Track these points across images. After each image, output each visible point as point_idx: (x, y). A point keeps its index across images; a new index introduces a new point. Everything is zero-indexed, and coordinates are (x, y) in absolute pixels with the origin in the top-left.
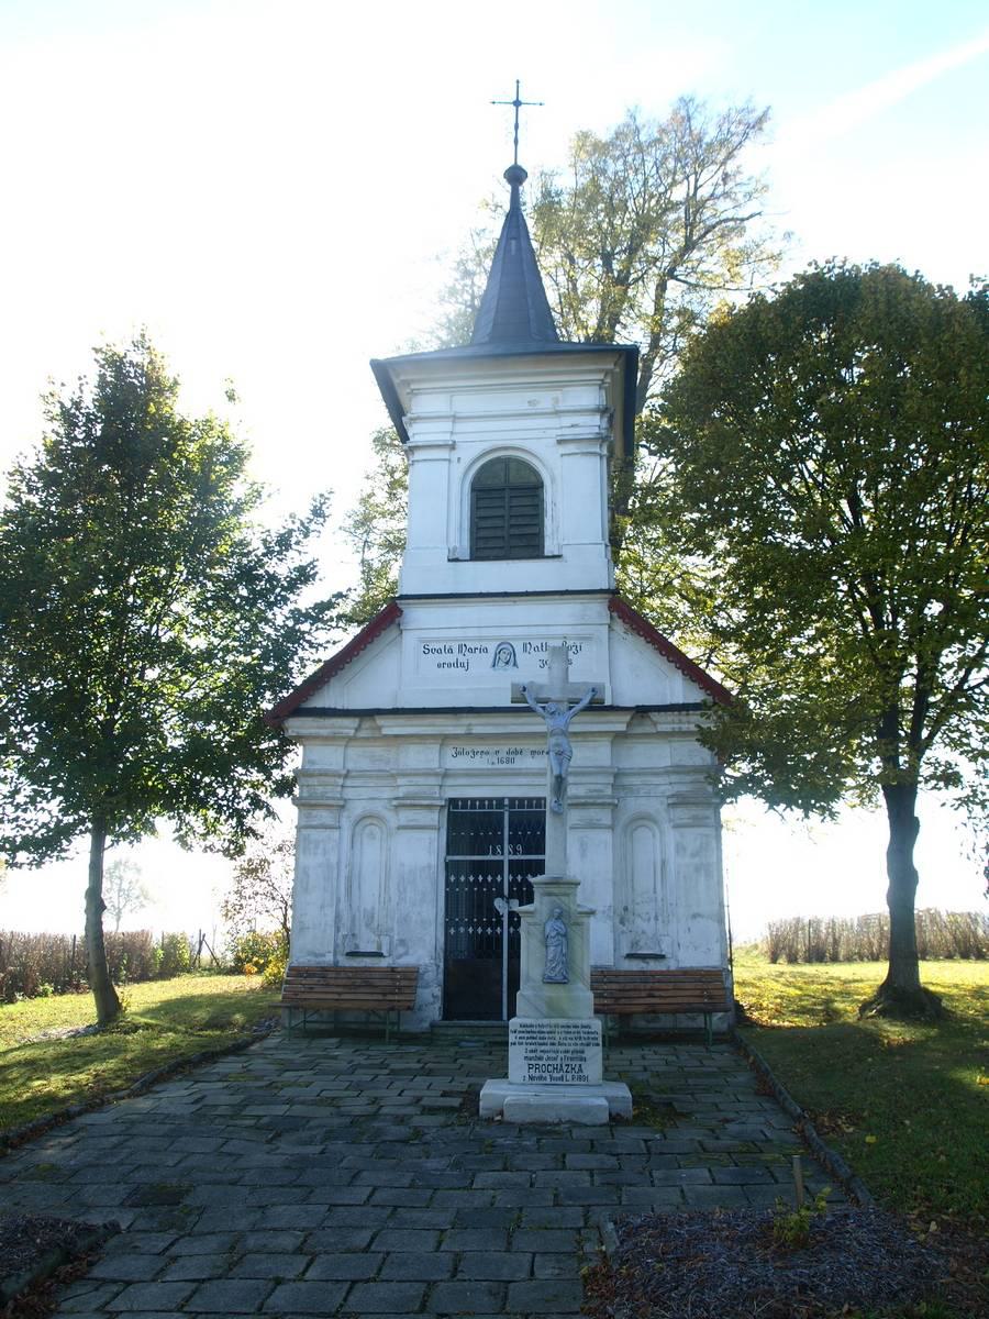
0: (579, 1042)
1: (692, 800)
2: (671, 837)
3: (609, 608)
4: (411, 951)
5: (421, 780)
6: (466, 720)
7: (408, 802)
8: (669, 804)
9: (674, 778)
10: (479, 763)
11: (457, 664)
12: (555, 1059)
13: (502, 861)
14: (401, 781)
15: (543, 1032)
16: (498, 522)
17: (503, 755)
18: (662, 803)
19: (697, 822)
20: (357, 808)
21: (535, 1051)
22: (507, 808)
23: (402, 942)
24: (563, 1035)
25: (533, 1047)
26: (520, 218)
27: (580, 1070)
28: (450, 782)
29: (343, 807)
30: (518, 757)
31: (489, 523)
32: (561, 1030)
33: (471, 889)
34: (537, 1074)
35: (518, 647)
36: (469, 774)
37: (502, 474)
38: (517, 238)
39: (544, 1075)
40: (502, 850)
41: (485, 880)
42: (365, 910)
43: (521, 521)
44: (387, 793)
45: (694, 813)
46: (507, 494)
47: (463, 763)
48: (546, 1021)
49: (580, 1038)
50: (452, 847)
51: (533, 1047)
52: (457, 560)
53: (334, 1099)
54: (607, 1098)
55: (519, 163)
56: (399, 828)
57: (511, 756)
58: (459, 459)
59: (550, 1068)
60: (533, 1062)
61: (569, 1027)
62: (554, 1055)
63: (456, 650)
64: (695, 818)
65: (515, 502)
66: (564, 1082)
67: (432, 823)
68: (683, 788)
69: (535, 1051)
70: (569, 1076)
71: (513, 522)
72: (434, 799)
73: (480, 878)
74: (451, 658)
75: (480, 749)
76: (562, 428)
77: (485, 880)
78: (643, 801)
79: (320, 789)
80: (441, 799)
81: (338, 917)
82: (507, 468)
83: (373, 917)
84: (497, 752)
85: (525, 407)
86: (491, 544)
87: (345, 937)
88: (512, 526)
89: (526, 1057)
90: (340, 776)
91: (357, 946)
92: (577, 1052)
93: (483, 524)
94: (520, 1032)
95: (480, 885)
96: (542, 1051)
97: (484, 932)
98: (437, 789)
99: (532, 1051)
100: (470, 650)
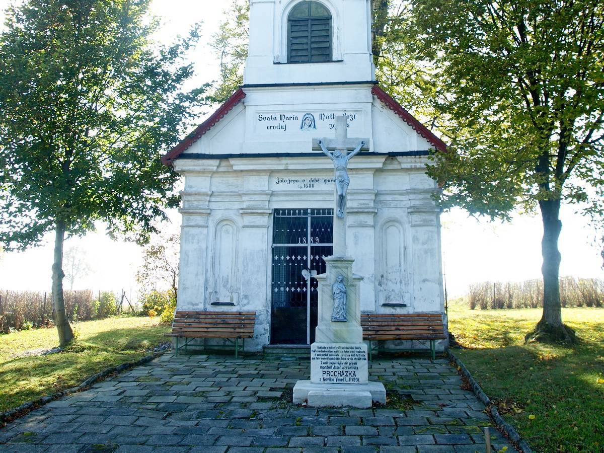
0: (353, 357)
2: (410, 232)
5: (257, 198)
6: (285, 161)
7: (249, 211)
8: (408, 213)
9: (412, 196)
10: (293, 187)
11: (279, 127)
12: (339, 368)
13: (306, 248)
14: (244, 198)
15: (332, 352)
16: (305, 40)
17: (306, 182)
18: (404, 212)
19: (425, 223)
20: (218, 215)
21: (327, 363)
22: (309, 215)
23: (246, 297)
24: (344, 353)
25: (326, 361)
27: (354, 374)
28: (275, 198)
29: (210, 214)
30: (316, 184)
32: (344, 350)
34: (328, 377)
36: (286, 194)
37: (307, 11)
39: (332, 378)
41: (296, 258)
42: (223, 277)
43: (318, 40)
44: (237, 206)
45: (424, 217)
46: (310, 21)
47: (283, 187)
48: (333, 345)
51: (326, 361)
57: (312, 183)
59: (336, 374)
62: (338, 366)
63: (278, 118)
65: (315, 28)
66: (345, 382)
68: (417, 203)
69: (327, 363)
70: (348, 378)
71: (313, 40)
73: (293, 258)
74: (275, 123)
77: (296, 258)
80: (269, 209)
81: (206, 281)
83: (228, 279)
84: (304, 181)
86: (300, 53)
87: (211, 293)
88: (312, 42)
90: (207, 195)
91: (218, 299)
95: (293, 262)
99: (325, 363)
100: (288, 118)
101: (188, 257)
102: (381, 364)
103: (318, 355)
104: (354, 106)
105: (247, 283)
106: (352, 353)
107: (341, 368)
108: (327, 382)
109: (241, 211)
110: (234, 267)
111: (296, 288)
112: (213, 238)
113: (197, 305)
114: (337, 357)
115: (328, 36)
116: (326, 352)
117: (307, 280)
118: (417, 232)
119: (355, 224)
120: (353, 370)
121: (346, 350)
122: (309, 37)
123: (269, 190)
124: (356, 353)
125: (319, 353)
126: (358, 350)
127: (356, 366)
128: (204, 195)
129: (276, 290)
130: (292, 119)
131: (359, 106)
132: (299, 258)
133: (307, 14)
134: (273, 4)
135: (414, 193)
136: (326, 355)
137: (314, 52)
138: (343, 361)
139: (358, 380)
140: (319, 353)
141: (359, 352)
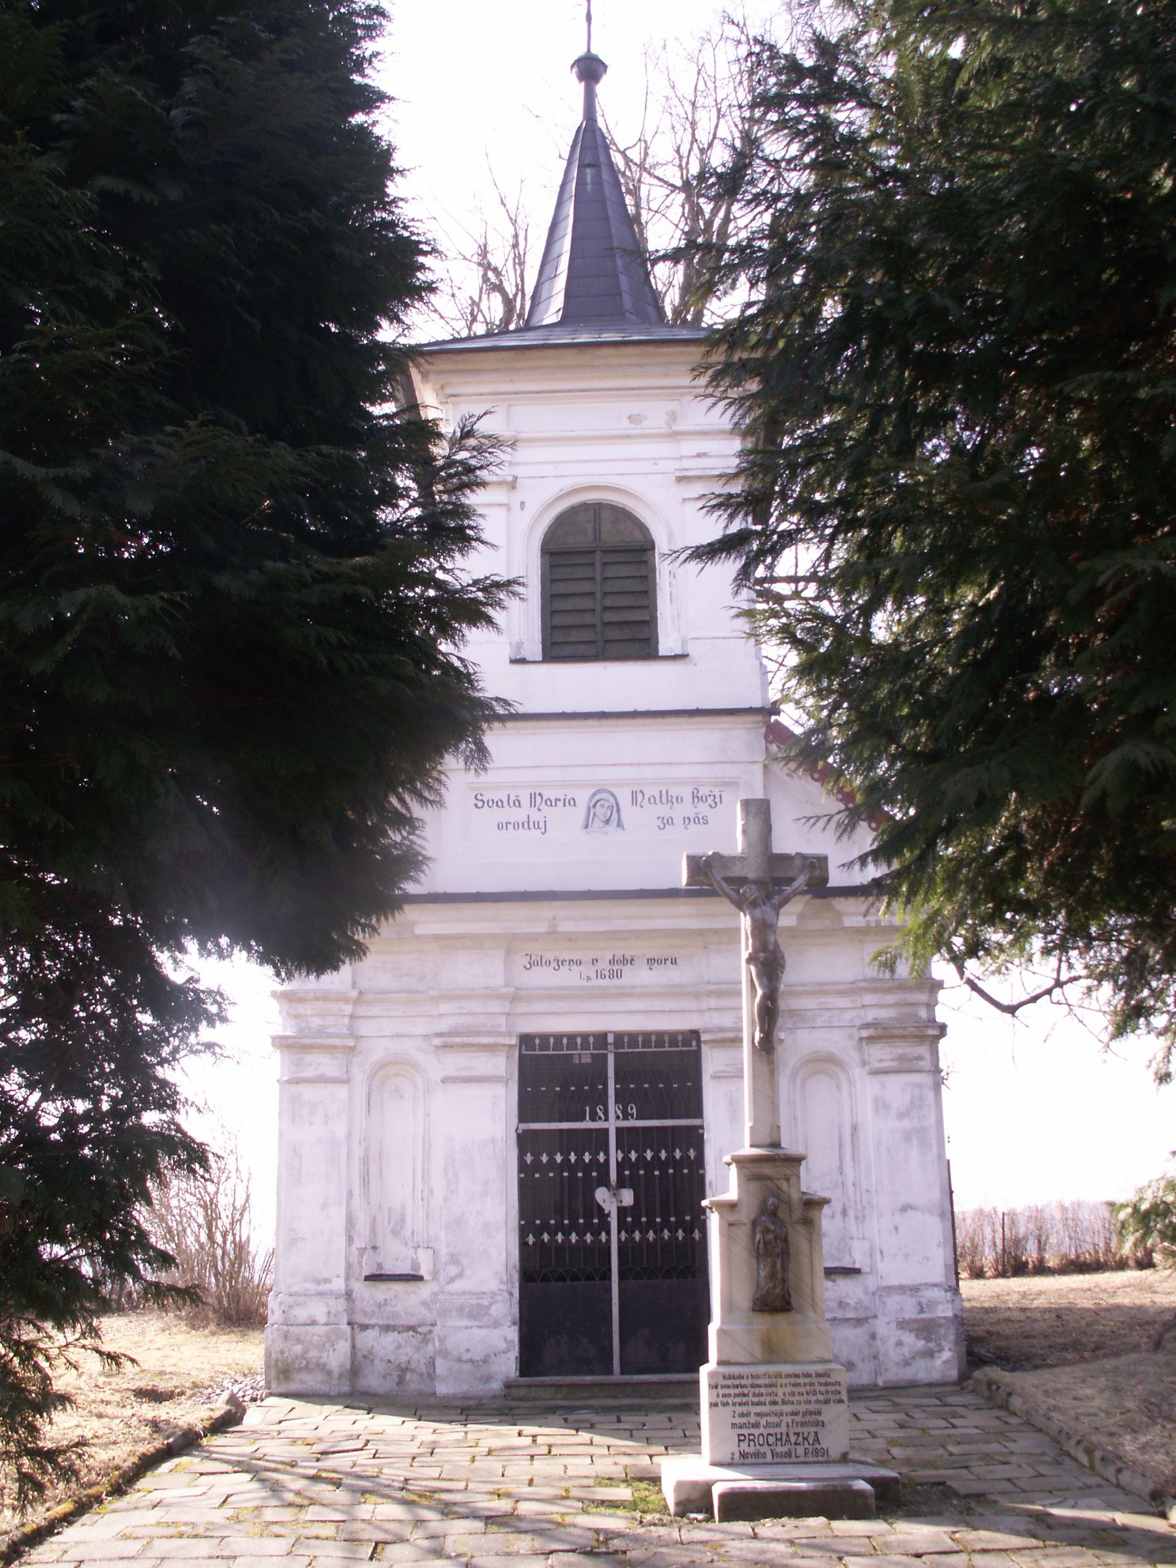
0: (813, 1398)
1: (896, 1032)
2: (867, 1088)
3: (766, 737)
4: (467, 1272)
5: (476, 1006)
6: (547, 911)
7: (458, 1040)
8: (861, 1039)
9: (869, 999)
10: (568, 977)
11: (527, 824)
12: (778, 1425)
13: (607, 1130)
14: (445, 1008)
15: (758, 1386)
16: (587, 603)
17: (603, 965)
18: (850, 1037)
19: (905, 1067)
20: (377, 1051)
21: (748, 1414)
22: (611, 1048)
23: (454, 1260)
24: (789, 1389)
25: (744, 1409)
26: (598, 132)
27: (817, 1440)
28: (522, 1008)
29: (352, 1049)
30: (627, 969)
31: (570, 604)
32: (787, 1381)
33: (573, 1175)
34: (752, 1449)
35: (624, 798)
36: (553, 995)
37: (590, 527)
38: (595, 165)
39: (762, 1450)
40: (606, 1113)
41: (580, 1159)
42: (390, 1209)
43: (619, 601)
44: (422, 1027)
45: (900, 1051)
46: (598, 557)
47: (543, 977)
48: (762, 1369)
49: (815, 1393)
50: (527, 1109)
51: (744, 1409)
52: (522, 661)
53: (434, 1491)
54: (871, 1481)
55: (594, 51)
56: (445, 1080)
57: (616, 967)
58: (522, 504)
59: (771, 1440)
60: (745, 1431)
61: (797, 1376)
62: (775, 1419)
63: (525, 801)
64: (901, 1058)
65: (611, 572)
66: (793, 1459)
67: (497, 1073)
68: (883, 1014)
69: (748, 1414)
70: (800, 1450)
71: (609, 602)
72: (501, 1034)
73: (573, 1157)
74: (519, 815)
75: (567, 955)
76: (681, 458)
77: (580, 1159)
78: (818, 1034)
79: (316, 1022)
80: (510, 1035)
81: (350, 1221)
82: (597, 520)
83: (403, 1221)
84: (595, 961)
85: (625, 427)
86: (574, 636)
87: (362, 1251)
88: (606, 609)
89: (734, 1425)
90: (346, 1000)
91: (380, 1266)
92: (811, 1413)
93: (560, 605)
94: (723, 1387)
95: (572, 1168)
96: (758, 1415)
97: (581, 1239)
98: (502, 1020)
99: (742, 1415)
100: (549, 803)
101: (301, 1158)
102: (623, 1418)
103: (724, 1396)
104: (718, 772)
105: (457, 1223)
106: (808, 1388)
107: (784, 1425)
108: (749, 1460)
109: (437, 1041)
110: (419, 1186)
111: (644, 1233)
112: (364, 1110)
113: (327, 1281)
114: (772, 1398)
115: (646, 592)
116: (745, 1386)
117: (609, 1215)
118: (884, 1087)
119: (729, 1069)
120: (812, 1429)
121: (792, 1380)
122: (598, 595)
123: (506, 985)
124: (818, 1388)
125: (726, 1391)
126: (823, 1380)
127: (820, 1418)
128: (338, 1000)
129: (531, 1240)
130: (560, 804)
131: (730, 772)
132: (587, 1157)
133: (591, 537)
134: (503, 511)
135: (875, 991)
136: (744, 1395)
137: (612, 634)
138: (787, 1408)
139: (826, 1452)
140: (726, 1391)
141: (826, 1384)
